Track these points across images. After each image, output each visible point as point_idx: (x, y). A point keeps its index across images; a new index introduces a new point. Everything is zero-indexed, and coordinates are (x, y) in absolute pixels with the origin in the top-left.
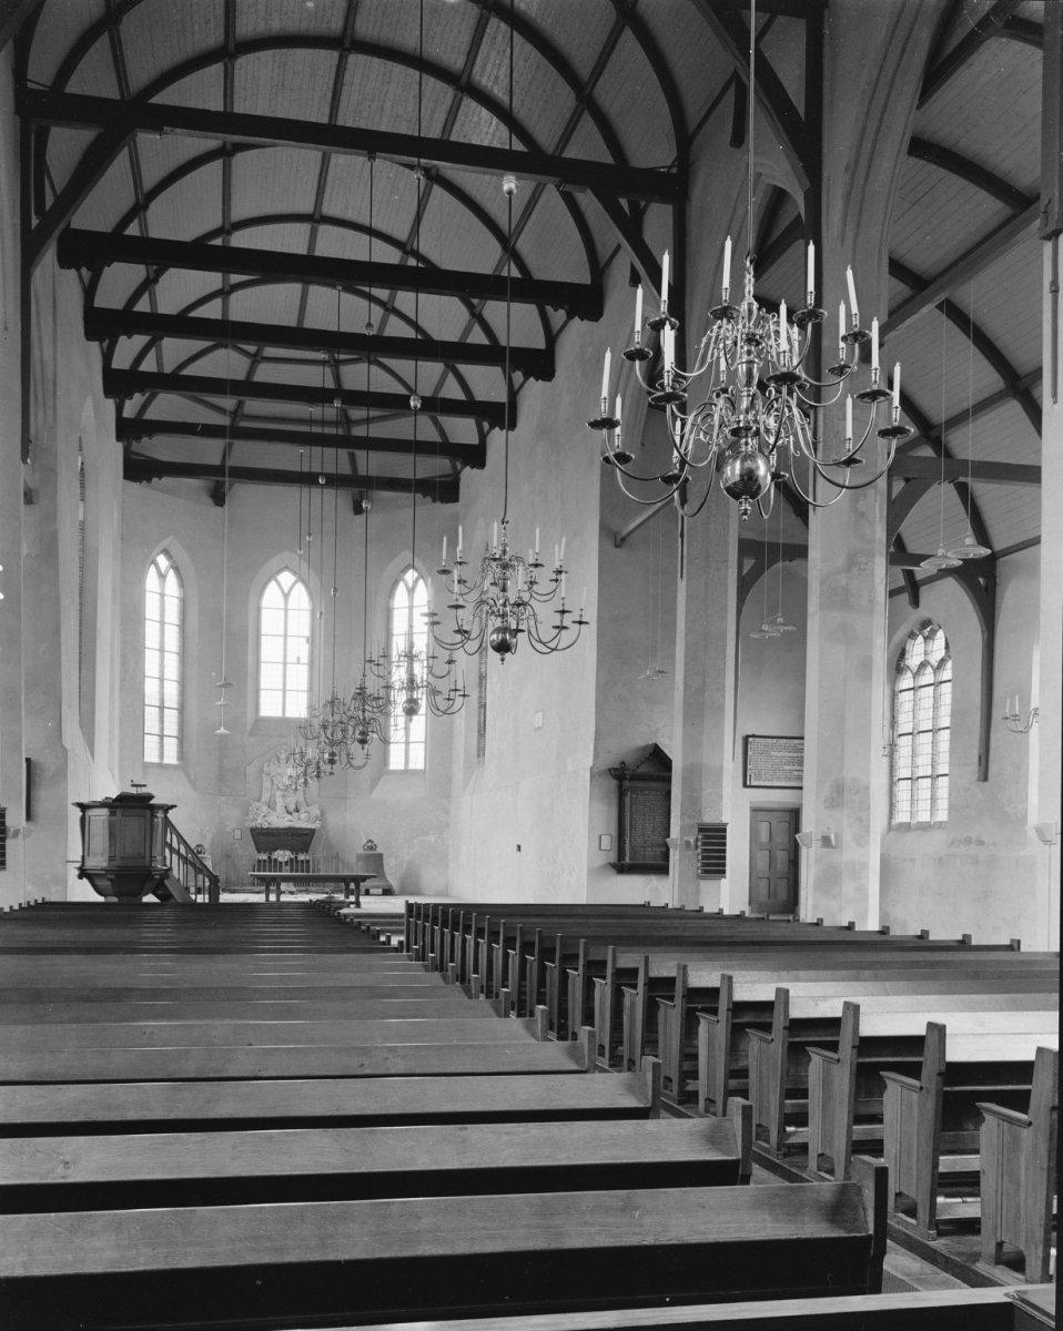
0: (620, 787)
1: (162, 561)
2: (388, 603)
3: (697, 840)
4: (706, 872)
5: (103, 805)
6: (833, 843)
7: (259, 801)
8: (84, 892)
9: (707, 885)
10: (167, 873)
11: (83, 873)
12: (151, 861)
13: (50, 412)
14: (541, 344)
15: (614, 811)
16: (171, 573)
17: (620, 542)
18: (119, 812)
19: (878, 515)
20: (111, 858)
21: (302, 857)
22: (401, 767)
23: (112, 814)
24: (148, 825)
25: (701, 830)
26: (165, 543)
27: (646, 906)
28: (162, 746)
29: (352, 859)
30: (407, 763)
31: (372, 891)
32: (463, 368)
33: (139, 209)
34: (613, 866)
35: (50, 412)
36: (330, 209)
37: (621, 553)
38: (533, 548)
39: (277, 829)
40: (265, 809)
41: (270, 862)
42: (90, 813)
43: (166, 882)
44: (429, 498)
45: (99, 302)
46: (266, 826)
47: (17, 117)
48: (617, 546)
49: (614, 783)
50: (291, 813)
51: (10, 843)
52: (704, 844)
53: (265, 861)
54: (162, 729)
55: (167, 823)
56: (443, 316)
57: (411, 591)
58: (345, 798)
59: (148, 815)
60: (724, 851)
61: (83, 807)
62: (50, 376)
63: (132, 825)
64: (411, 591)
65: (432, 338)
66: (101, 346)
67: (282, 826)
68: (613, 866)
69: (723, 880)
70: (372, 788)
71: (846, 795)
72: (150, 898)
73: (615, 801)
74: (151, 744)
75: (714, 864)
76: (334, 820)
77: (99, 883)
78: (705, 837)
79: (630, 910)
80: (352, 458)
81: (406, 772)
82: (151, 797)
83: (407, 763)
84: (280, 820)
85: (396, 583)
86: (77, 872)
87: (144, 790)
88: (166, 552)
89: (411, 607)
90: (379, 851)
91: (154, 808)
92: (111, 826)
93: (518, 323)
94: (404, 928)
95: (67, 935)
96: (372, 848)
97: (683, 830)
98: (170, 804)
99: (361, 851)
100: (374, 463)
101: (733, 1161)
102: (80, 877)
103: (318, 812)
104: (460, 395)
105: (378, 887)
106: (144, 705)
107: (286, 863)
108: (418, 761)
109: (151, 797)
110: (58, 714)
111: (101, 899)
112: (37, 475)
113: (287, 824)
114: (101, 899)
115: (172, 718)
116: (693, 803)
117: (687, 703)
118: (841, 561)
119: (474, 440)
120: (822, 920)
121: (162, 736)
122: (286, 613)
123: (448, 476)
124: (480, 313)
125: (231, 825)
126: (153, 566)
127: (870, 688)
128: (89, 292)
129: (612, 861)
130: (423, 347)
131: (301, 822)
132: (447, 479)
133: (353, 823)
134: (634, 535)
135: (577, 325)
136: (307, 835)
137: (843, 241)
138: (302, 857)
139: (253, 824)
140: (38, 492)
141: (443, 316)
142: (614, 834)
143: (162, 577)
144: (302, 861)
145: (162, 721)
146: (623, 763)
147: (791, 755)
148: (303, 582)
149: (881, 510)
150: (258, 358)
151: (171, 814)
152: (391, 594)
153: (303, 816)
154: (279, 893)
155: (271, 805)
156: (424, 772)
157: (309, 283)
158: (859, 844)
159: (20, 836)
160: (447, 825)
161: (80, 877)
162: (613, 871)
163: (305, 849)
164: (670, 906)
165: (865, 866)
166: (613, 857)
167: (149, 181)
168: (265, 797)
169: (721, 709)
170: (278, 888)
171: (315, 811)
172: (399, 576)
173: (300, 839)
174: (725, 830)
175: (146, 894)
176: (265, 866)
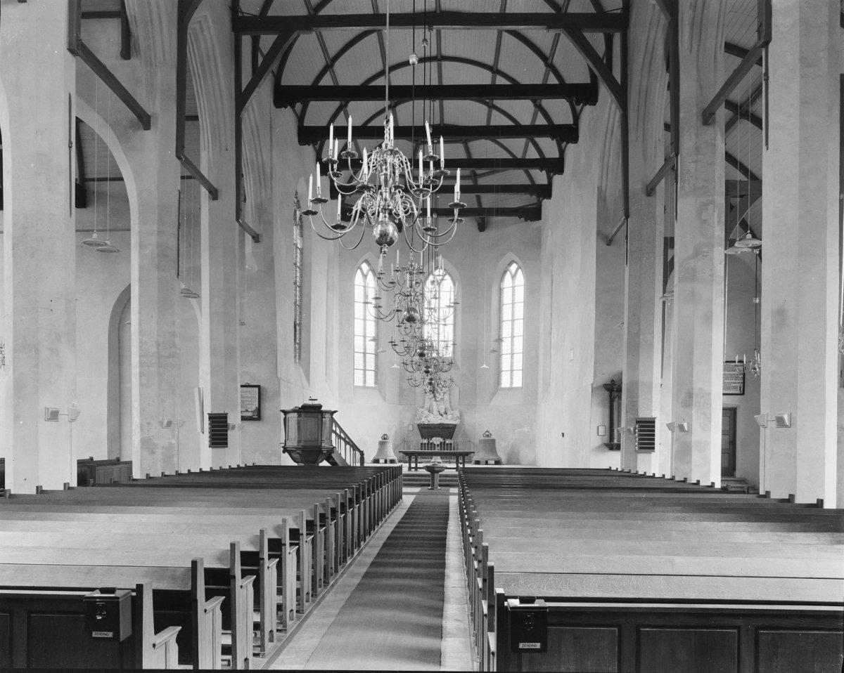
0: (611, 396)
1: (365, 267)
2: (500, 285)
3: (635, 428)
4: (641, 448)
5: (294, 411)
6: (686, 429)
7: (423, 407)
8: (287, 461)
9: (642, 457)
10: (332, 450)
11: (285, 450)
12: (321, 443)
13: (269, 190)
14: (571, 121)
15: (607, 411)
16: (370, 273)
17: (609, 242)
18: (303, 415)
19: (716, 220)
20: (299, 441)
21: (448, 441)
22: (508, 386)
23: (299, 416)
24: (320, 421)
25: (637, 422)
26: (366, 256)
27: (610, 469)
28: (365, 376)
29: (477, 442)
30: (512, 383)
31: (489, 462)
32: (538, 140)
33: (329, 67)
34: (606, 445)
35: (269, 190)
36: (445, 52)
37: (612, 249)
38: (395, 263)
39: (433, 425)
40: (427, 412)
41: (444, 444)
42: (288, 415)
43: (333, 455)
44: (522, 219)
45: (307, 123)
46: (426, 423)
47: (233, 33)
48: (608, 245)
49: (607, 393)
50: (442, 415)
51: (230, 433)
52: (640, 431)
53: (425, 444)
54: (365, 366)
55: (333, 421)
56: (523, 111)
57: (513, 277)
58: (475, 406)
59: (320, 416)
60: (654, 435)
61: (285, 412)
62: (268, 170)
63: (311, 422)
64: (513, 277)
65: (520, 125)
66: (315, 148)
67: (436, 423)
68: (606, 445)
69: (653, 453)
70: (491, 399)
71: (694, 399)
72: (325, 463)
73: (608, 405)
74: (358, 375)
75: (647, 443)
76: (468, 419)
77: (294, 455)
78: (641, 426)
79: (583, 471)
80: (479, 199)
81: (511, 389)
82: (321, 406)
83: (512, 383)
84: (435, 419)
85: (505, 272)
86: (282, 449)
87: (316, 403)
88: (366, 261)
89: (514, 285)
90: (493, 437)
91: (322, 413)
92: (299, 423)
93: (559, 110)
94: (430, 483)
95: (263, 480)
96: (488, 436)
97: (628, 423)
98: (333, 410)
99: (482, 438)
100: (488, 200)
101: (227, 569)
102: (284, 452)
103: (458, 414)
104: (537, 156)
105: (492, 460)
106: (354, 352)
107: (438, 445)
108: (518, 383)
109: (321, 406)
110: (275, 362)
111: (296, 464)
112: (262, 226)
113: (439, 422)
114: (296, 464)
115: (371, 359)
116: (634, 405)
117: (629, 343)
118: (691, 252)
119: (545, 182)
120: (664, 475)
121: (365, 370)
122: (442, 293)
123: (535, 204)
124: (540, 105)
125: (407, 422)
126: (359, 270)
127: (711, 330)
128: (301, 119)
129: (606, 442)
130: (516, 130)
131: (448, 420)
132: (534, 206)
133: (480, 421)
134: (617, 236)
135: (588, 108)
136: (451, 428)
137: (691, 51)
138: (448, 441)
139: (419, 422)
140: (262, 235)
141: (523, 111)
142: (607, 424)
143: (365, 276)
144: (447, 444)
145: (365, 361)
146: (613, 381)
147: (729, 373)
148: (450, 275)
149: (719, 216)
150: (419, 142)
151: (335, 416)
152: (502, 279)
153: (449, 417)
154: (464, 463)
155: (430, 411)
156: (522, 388)
157: (443, 100)
158: (703, 429)
159: (236, 429)
160: (535, 421)
161: (284, 452)
162: (607, 449)
163: (450, 437)
164: (657, 476)
165: (708, 443)
166: (606, 440)
167: (332, 53)
168: (427, 405)
169: (651, 346)
170: (416, 459)
171: (457, 413)
172: (506, 268)
173: (447, 431)
174: (654, 422)
175: (322, 461)
176: (425, 447)
